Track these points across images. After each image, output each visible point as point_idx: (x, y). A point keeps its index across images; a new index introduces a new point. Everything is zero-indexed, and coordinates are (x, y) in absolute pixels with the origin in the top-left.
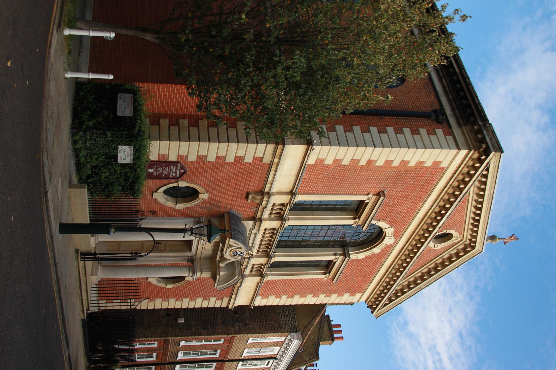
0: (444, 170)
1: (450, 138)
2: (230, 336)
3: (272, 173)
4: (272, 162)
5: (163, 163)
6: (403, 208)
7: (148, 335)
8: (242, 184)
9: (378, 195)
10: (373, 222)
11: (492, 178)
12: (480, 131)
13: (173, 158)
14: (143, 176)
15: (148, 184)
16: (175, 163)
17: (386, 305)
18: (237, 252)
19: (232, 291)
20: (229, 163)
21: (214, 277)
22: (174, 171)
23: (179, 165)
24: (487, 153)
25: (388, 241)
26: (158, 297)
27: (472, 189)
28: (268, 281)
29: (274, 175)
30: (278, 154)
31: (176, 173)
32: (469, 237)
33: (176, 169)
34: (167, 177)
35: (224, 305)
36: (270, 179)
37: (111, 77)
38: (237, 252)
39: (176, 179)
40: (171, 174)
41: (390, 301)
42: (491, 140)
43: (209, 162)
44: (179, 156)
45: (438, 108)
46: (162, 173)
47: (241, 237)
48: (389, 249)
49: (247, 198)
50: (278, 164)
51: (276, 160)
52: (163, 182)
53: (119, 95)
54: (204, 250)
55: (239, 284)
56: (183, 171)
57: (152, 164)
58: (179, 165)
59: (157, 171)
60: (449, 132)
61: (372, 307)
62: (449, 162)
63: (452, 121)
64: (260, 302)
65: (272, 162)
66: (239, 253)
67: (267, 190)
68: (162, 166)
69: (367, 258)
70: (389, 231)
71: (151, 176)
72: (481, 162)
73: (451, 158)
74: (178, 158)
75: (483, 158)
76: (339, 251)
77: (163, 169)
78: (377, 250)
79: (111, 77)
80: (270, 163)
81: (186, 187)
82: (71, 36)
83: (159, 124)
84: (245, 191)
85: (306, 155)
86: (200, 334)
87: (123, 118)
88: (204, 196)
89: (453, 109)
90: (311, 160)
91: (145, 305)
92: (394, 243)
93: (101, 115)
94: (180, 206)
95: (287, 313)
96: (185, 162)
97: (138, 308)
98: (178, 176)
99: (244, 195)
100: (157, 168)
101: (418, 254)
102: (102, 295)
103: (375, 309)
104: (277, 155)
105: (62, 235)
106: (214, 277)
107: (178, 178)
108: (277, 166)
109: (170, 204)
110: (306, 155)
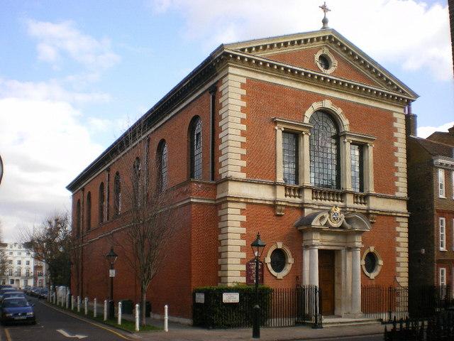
0: (249, 80)
1: (224, 81)
2: (435, 213)
3: (254, 201)
4: (244, 202)
5: (248, 273)
6: (291, 100)
7: (431, 275)
9: (276, 123)
10: (306, 121)
11: (250, 44)
12: (216, 61)
13: (244, 268)
15: (268, 283)
16: (248, 266)
17: (403, 92)
19: (390, 216)
21: (360, 233)
24: (227, 54)
25: (328, 104)
26: (394, 270)
27: (259, 56)
28: (375, 190)
32: (321, 42)
35: (406, 220)
36: (261, 202)
37: (166, 306)
39: (264, 264)
41: (398, 89)
42: (218, 53)
45: (208, 92)
48: (336, 102)
49: (281, 216)
52: (266, 272)
53: (203, 302)
55: (378, 212)
60: (219, 82)
61: (409, 102)
63: (215, 80)
64: (402, 192)
65: (244, 202)
67: (271, 203)
69: (348, 117)
70: (316, 106)
72: (235, 56)
73: (235, 81)
75: (231, 56)
76: (342, 140)
78: (339, 111)
79: (166, 306)
82: (168, 327)
83: (220, 277)
85: (237, 181)
86: (433, 236)
87: (206, 298)
88: (280, 245)
89: (210, 81)
90: (243, 176)
91: (403, 280)
92: (329, 99)
93: (208, 313)
94: (291, 260)
95: (419, 169)
97: (406, 284)
99: (279, 218)
101: (337, 79)
103: (408, 100)
104: (237, 200)
105: (261, 335)
106: (360, 233)
108: (248, 199)
109: (288, 268)
110: (237, 181)
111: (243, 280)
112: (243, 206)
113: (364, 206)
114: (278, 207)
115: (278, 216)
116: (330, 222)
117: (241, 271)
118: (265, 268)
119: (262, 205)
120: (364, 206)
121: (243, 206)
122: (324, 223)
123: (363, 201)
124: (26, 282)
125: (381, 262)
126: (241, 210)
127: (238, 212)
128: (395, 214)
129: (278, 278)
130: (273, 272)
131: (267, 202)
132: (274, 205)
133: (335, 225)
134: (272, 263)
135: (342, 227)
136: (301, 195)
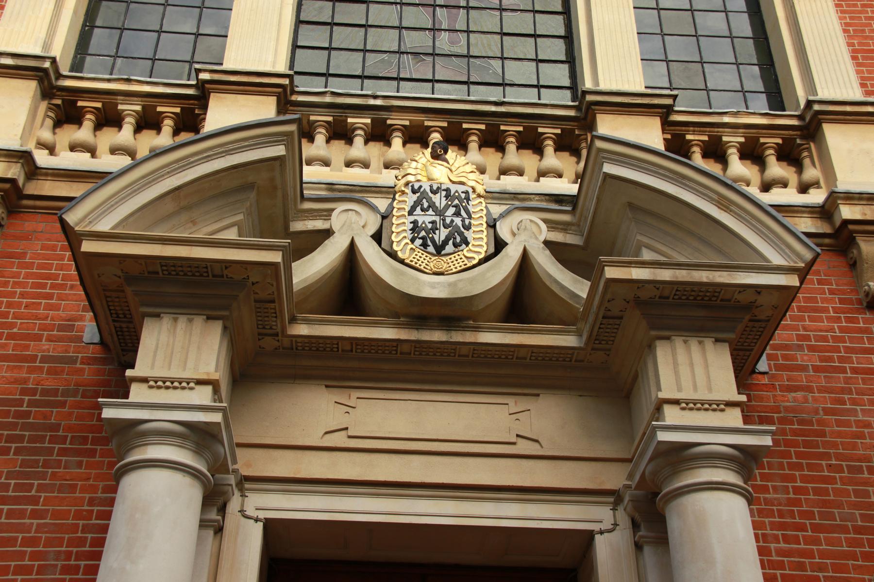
18: (415, 227)
54: (523, 447)
66: (425, 219)
116: (372, 256)
133: (433, 282)
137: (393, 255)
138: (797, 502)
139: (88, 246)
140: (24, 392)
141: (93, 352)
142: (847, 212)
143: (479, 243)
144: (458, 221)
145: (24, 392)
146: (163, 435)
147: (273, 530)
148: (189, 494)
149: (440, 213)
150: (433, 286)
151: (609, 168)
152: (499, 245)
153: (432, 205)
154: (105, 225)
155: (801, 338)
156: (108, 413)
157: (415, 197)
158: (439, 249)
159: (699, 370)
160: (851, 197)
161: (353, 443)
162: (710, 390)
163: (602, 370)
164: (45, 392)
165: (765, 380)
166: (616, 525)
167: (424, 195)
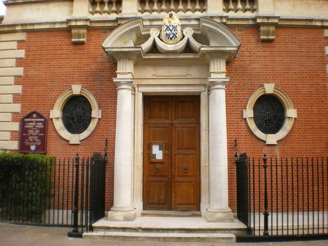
3: (36, 27)
4: (23, 31)
8: (60, 52)
13: (16, 127)
14: (38, 157)
16: (23, 123)
18: (167, 35)
20: (25, 71)
22: (34, 125)
23: (26, 120)
29: (40, 24)
30: (10, 29)
31: (37, 122)
33: (32, 122)
34: (44, 130)
36: (304, 23)
38: (167, 35)
39: (47, 122)
40: (39, 127)
43: (23, 91)
44: (13, 121)
46: (38, 135)
47: (100, 149)
49: (83, 43)
50: (22, 25)
51: (19, 28)
52: (51, 134)
54: (189, 77)
56: (35, 115)
57: (24, 147)
58: (26, 120)
59: (34, 141)
62: (294, 219)
66: (168, 32)
67: (64, 26)
68: (27, 137)
71: (42, 148)
74: (17, 121)
77: (31, 135)
80: (26, 32)
81: (255, 109)
84: (71, 47)
88: (77, 89)
96: (22, 114)
98: (42, 120)
99: (79, 47)
100: (29, 141)
102: (321, 205)
107: (45, 119)
108: (26, 25)
111: (14, 145)
112: (22, 37)
113: (249, 14)
114: (262, 28)
115: (264, 41)
116: (160, 43)
117: (11, 131)
118: (50, 128)
119: (51, 31)
120: (249, 14)
121: (22, 37)
122: (146, 45)
123: (248, 6)
124: (29, 174)
125: (291, 113)
126: (19, 41)
127: (15, 45)
128: (319, 24)
129: (268, 143)
130: (259, 134)
131: (57, 26)
132: (67, 30)
133: (170, 47)
134: (256, 119)
135: (188, 48)
136: (255, 7)
137: (162, 41)
138: (239, 85)
139: (106, 50)
140: (97, 69)
141: (108, 60)
142: (259, 21)
143: (179, 35)
144: (175, 33)
145: (97, 69)
146: (124, 84)
147: (143, 93)
148: (130, 92)
149: (171, 31)
150: (171, 47)
151: (204, 24)
152: (184, 36)
153: (169, 29)
154: (108, 46)
155: (246, 49)
156: (114, 80)
157: (166, 27)
158: (171, 39)
159: (219, 65)
160: (260, 17)
161: (157, 77)
162: (220, 69)
163: (203, 61)
164: (101, 69)
165: (237, 59)
166: (175, 155)
167: (168, 27)
